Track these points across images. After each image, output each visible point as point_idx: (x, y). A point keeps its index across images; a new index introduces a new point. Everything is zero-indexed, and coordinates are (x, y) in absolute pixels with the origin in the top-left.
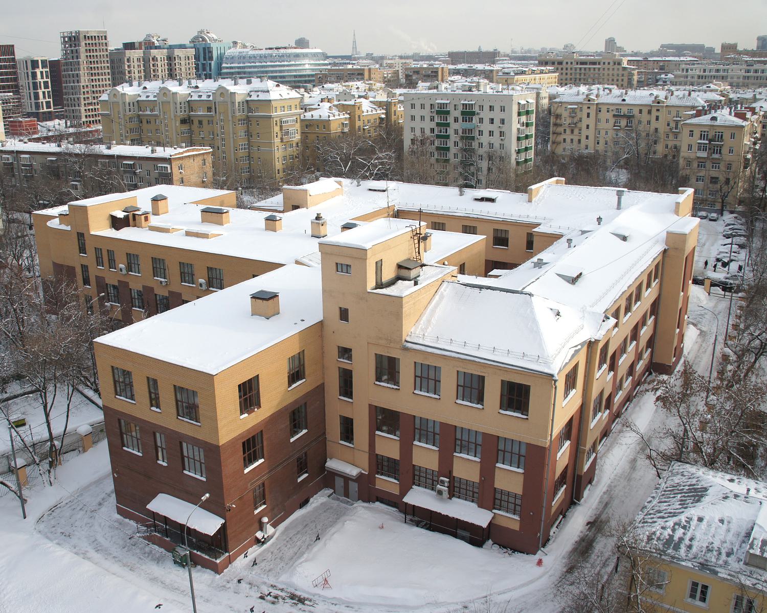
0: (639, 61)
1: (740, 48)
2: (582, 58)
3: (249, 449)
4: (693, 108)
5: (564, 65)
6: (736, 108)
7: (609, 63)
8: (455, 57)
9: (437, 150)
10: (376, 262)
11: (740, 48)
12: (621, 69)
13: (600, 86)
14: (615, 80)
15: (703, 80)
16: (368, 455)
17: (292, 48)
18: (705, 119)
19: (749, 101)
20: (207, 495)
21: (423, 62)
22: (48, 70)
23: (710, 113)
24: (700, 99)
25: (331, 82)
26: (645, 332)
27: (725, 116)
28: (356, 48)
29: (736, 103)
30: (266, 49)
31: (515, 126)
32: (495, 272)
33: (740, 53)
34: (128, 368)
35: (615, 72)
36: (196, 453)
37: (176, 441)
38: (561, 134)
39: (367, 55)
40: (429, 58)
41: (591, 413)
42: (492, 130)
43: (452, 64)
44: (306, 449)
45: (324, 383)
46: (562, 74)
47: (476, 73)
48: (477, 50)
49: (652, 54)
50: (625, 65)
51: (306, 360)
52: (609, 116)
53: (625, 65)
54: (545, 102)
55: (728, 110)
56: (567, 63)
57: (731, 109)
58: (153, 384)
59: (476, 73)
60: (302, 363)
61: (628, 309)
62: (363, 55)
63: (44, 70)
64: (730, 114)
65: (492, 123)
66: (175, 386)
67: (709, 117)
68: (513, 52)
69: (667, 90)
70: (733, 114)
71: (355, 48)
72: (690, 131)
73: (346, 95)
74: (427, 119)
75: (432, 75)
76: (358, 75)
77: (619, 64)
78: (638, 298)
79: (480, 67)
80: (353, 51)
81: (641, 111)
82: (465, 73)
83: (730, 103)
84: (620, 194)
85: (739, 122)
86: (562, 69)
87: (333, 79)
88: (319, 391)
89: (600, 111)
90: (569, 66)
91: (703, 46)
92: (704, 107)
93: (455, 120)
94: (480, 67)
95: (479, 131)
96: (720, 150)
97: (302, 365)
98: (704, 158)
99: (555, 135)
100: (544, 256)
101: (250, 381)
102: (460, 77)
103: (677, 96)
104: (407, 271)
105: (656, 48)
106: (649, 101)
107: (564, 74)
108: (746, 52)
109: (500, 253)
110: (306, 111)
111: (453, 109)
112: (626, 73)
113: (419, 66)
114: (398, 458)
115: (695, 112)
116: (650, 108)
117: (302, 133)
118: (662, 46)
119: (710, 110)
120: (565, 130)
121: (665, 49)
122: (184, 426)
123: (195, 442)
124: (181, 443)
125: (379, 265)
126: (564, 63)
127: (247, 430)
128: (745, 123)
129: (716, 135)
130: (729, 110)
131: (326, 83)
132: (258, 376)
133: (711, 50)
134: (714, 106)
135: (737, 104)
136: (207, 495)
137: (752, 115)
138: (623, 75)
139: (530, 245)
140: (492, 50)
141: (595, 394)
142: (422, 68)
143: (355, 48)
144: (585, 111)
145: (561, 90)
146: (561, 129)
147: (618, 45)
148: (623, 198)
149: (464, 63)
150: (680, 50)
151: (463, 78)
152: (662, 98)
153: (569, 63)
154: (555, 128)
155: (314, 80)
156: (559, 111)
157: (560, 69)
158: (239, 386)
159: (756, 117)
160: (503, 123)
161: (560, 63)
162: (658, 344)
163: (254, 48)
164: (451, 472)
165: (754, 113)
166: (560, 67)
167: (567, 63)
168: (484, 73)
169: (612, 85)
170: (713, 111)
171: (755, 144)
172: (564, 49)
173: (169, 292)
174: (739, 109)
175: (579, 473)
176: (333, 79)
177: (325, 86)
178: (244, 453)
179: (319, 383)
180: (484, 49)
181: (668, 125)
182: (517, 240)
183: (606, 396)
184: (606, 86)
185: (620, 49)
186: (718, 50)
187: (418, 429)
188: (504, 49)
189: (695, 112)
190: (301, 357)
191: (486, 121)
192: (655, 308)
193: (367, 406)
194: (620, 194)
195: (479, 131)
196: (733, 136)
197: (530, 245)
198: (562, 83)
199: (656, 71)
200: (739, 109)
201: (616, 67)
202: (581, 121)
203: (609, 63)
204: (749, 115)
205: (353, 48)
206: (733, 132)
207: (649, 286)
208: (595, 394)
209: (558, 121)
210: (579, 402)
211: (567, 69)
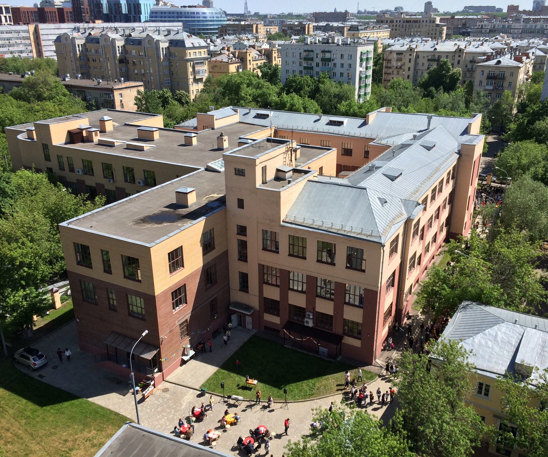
0: (448, 19)
1: (521, 9)
2: (407, 17)
3: (177, 301)
4: (484, 54)
5: (395, 23)
6: (515, 53)
7: (426, 21)
8: (317, 17)
9: (322, 61)
10: (262, 168)
11: (521, 9)
12: (435, 26)
13: (419, 39)
14: (430, 34)
15: (493, 32)
16: (258, 297)
17: (200, 7)
18: (493, 62)
19: (525, 48)
20: (147, 331)
21: (295, 20)
22: (11, 15)
23: (496, 58)
24: (487, 48)
25: (229, 35)
26: (445, 215)
27: (507, 60)
28: (247, 8)
29: (516, 50)
30: (181, 7)
31: (358, 69)
32: (343, 173)
33: (520, 12)
34: (85, 243)
35: (431, 28)
36: (139, 301)
37: (124, 293)
38: (390, 74)
39: (255, 13)
40: (298, 16)
41: (408, 268)
42: (342, 72)
43: (316, 22)
44: (216, 295)
45: (227, 251)
46: (393, 29)
47: (332, 29)
48: (333, 11)
49: (458, 13)
50: (438, 22)
51: (215, 235)
52: (425, 61)
53: (438, 22)
54: (380, 50)
55: (509, 55)
56: (397, 21)
57: (511, 54)
58: (105, 253)
59: (332, 29)
60: (212, 237)
61: (433, 198)
62: (252, 13)
63: (7, 15)
64: (511, 58)
65: (343, 67)
66: (122, 255)
67: (495, 61)
68: (359, 12)
69: (467, 41)
70: (513, 58)
71: (246, 8)
72: (482, 71)
73: (239, 45)
74: (298, 64)
75: (301, 30)
76: (247, 29)
77: (434, 22)
78: (440, 190)
79: (335, 24)
80: (245, 11)
81: (447, 57)
82: (325, 29)
83: (512, 50)
84: (430, 119)
85: (515, 64)
86: (393, 26)
87: (230, 32)
88: (225, 255)
89: (418, 57)
90: (398, 24)
91: (495, 7)
92: (492, 53)
93: (317, 65)
94: (335, 24)
95: (334, 73)
96: (502, 84)
97: (212, 239)
98: (491, 90)
99: (387, 75)
100: (375, 162)
101: (176, 250)
102: (321, 32)
103: (474, 46)
104: (283, 173)
105: (461, 9)
106: (453, 49)
107: (394, 29)
108: (525, 12)
109: (347, 161)
110: (211, 56)
111: (316, 57)
112: (438, 28)
113: (292, 23)
114: (279, 300)
115: (486, 57)
116: (453, 55)
117: (209, 72)
118: (466, 7)
119: (496, 56)
120: (393, 71)
121: (467, 10)
122: (130, 285)
123: (138, 294)
124: (127, 295)
125: (264, 169)
126: (395, 22)
127: (175, 284)
128: (521, 65)
129: (500, 73)
130: (510, 56)
131: (225, 35)
132: (182, 247)
133: (500, 10)
134: (500, 52)
135: (516, 51)
136: (147, 331)
137: (526, 59)
138: (436, 29)
139: (367, 153)
140: (343, 11)
141: (410, 255)
142: (294, 25)
143: (246, 8)
144: (408, 57)
145: (391, 42)
146: (390, 71)
147: (434, 7)
148: (432, 120)
149: (324, 21)
150: (477, 9)
151: (323, 33)
152: (462, 47)
153: (398, 21)
154: (386, 70)
155: (217, 32)
156: (389, 58)
157: (391, 26)
158: (169, 254)
159: (528, 60)
160: (350, 67)
161: (392, 22)
162: (453, 222)
163: (172, 6)
164: (314, 308)
165: (528, 57)
166: (392, 24)
167: (397, 21)
168: (338, 29)
169: (428, 37)
170: (498, 56)
171: (527, 79)
172: (395, 10)
173: (116, 188)
174: (517, 54)
175: (401, 308)
176: (230, 32)
177: (225, 37)
178: (173, 300)
179: (225, 250)
180: (338, 10)
181: (466, 66)
182: (358, 153)
183: (417, 256)
184: (424, 39)
185: (436, 10)
186: (505, 10)
187: (291, 280)
188: (353, 10)
189: (486, 57)
190: (212, 232)
191: (338, 65)
192: (452, 195)
193: (257, 265)
194: (430, 119)
195: (334, 73)
196: (512, 74)
197: (367, 153)
198: (392, 37)
199: (460, 26)
200: (517, 54)
201: (431, 24)
202: (404, 64)
203: (426, 21)
204: (524, 58)
205: (245, 8)
206: (512, 71)
207: (448, 182)
208: (410, 255)
209: (389, 65)
210: (399, 261)
211: (396, 26)
